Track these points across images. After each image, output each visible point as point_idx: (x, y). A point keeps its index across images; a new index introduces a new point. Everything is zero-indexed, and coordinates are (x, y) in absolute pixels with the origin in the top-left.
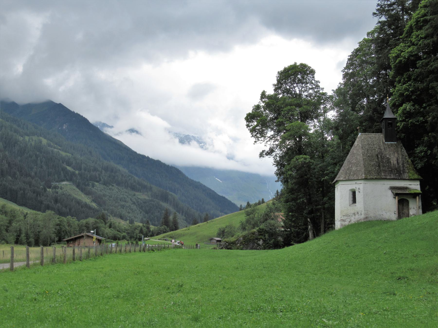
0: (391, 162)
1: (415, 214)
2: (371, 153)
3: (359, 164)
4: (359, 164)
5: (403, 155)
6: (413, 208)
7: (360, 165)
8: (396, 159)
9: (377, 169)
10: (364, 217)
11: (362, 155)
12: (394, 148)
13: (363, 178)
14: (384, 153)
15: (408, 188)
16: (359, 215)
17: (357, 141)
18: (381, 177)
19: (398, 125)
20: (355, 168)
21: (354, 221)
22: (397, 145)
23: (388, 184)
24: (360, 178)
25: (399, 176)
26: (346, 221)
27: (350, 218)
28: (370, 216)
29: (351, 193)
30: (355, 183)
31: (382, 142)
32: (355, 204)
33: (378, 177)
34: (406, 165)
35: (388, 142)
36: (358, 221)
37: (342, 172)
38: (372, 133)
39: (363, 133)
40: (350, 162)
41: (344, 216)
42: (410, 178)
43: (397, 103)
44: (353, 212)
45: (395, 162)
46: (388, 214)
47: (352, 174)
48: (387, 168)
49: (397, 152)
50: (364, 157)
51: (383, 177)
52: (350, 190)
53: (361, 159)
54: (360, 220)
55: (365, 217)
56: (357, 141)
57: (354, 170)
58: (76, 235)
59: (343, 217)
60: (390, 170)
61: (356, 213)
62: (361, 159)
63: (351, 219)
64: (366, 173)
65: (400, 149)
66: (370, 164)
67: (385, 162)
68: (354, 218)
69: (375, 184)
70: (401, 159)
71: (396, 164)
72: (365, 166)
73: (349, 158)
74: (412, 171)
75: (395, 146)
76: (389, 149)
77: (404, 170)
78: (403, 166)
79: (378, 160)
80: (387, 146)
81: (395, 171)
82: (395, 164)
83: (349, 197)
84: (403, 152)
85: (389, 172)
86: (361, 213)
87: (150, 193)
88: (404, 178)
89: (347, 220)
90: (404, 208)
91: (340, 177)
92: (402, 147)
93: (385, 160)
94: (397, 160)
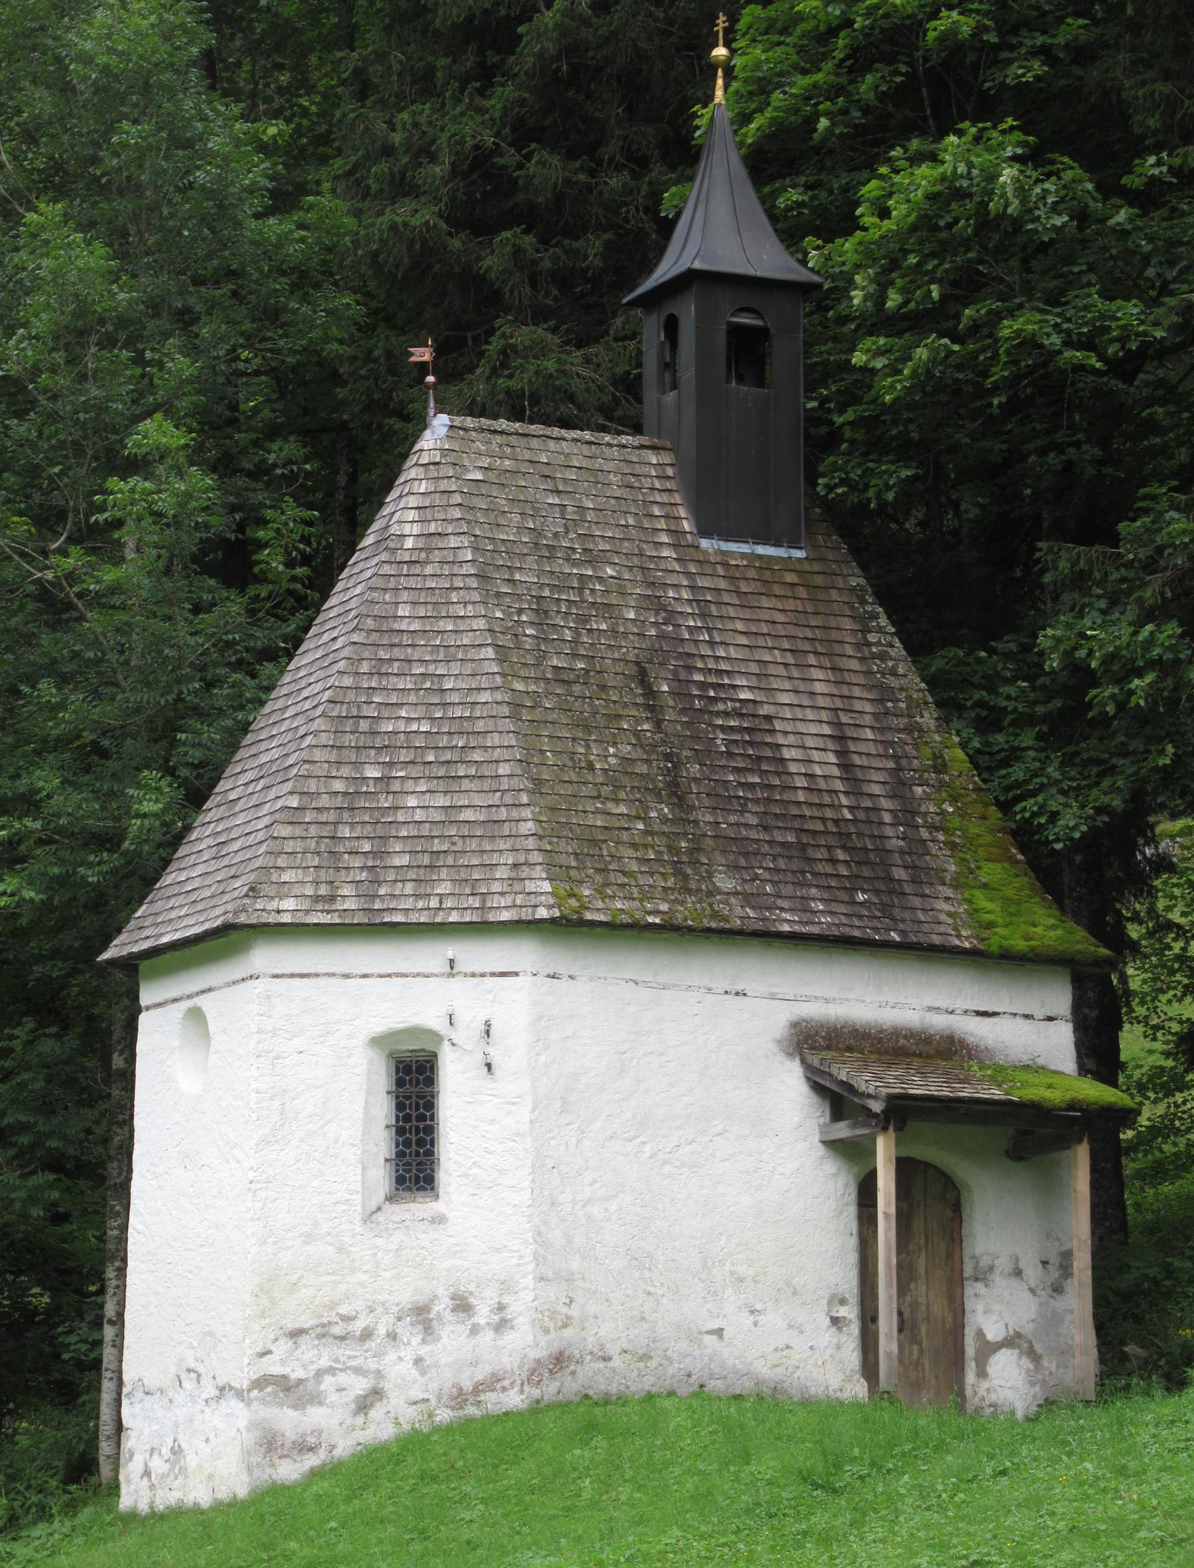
0: (787, 754)
1: (1028, 1329)
2: (575, 642)
3: (477, 756)
4: (477, 756)
5: (884, 694)
6: (1003, 1263)
7: (486, 771)
8: (827, 730)
9: (665, 820)
10: (534, 1354)
11: (490, 652)
12: (790, 604)
13: (542, 913)
14: (705, 650)
15: (962, 1042)
16: (474, 1331)
17: (413, 501)
18: (715, 915)
19: (858, 358)
20: (427, 800)
21: (417, 1393)
22: (819, 580)
23: (773, 997)
24: (505, 916)
25: (885, 908)
26: (316, 1399)
27: (372, 1364)
28: (591, 1343)
29: (382, 1080)
30: (441, 966)
31: (664, 538)
32: (419, 1208)
33: (687, 911)
34: (927, 797)
35: (727, 536)
36: (460, 1398)
37: (285, 831)
38: (556, 431)
39: (469, 422)
40: (364, 725)
41: (296, 1334)
42: (994, 945)
43: (824, 123)
44: (406, 1297)
45: (826, 764)
46: (773, 1320)
47: (405, 860)
48: (753, 820)
49: (830, 654)
50: (519, 686)
51: (740, 914)
52: (377, 1041)
53: (485, 697)
54: (493, 1382)
56: (413, 501)
57: (419, 815)
59: (285, 1345)
60: (791, 838)
61: (437, 1308)
62: (485, 697)
63: (379, 1374)
64: (563, 860)
65: (848, 624)
66: (591, 767)
67: (730, 755)
68: (418, 1361)
69: (648, 985)
70: (869, 734)
71: (839, 786)
72: (538, 782)
73: (347, 681)
74: (991, 872)
75: (802, 592)
76: (748, 614)
77: (917, 847)
78: (907, 814)
79: (658, 724)
80: (722, 584)
81: (833, 861)
82: (822, 784)
83: (367, 1118)
84: (883, 657)
85: (782, 864)
86: (501, 1308)
87: (1060, 626)
88: (936, 940)
89: (328, 1382)
91: (267, 889)
92: (863, 602)
93: (723, 728)
94: (841, 739)
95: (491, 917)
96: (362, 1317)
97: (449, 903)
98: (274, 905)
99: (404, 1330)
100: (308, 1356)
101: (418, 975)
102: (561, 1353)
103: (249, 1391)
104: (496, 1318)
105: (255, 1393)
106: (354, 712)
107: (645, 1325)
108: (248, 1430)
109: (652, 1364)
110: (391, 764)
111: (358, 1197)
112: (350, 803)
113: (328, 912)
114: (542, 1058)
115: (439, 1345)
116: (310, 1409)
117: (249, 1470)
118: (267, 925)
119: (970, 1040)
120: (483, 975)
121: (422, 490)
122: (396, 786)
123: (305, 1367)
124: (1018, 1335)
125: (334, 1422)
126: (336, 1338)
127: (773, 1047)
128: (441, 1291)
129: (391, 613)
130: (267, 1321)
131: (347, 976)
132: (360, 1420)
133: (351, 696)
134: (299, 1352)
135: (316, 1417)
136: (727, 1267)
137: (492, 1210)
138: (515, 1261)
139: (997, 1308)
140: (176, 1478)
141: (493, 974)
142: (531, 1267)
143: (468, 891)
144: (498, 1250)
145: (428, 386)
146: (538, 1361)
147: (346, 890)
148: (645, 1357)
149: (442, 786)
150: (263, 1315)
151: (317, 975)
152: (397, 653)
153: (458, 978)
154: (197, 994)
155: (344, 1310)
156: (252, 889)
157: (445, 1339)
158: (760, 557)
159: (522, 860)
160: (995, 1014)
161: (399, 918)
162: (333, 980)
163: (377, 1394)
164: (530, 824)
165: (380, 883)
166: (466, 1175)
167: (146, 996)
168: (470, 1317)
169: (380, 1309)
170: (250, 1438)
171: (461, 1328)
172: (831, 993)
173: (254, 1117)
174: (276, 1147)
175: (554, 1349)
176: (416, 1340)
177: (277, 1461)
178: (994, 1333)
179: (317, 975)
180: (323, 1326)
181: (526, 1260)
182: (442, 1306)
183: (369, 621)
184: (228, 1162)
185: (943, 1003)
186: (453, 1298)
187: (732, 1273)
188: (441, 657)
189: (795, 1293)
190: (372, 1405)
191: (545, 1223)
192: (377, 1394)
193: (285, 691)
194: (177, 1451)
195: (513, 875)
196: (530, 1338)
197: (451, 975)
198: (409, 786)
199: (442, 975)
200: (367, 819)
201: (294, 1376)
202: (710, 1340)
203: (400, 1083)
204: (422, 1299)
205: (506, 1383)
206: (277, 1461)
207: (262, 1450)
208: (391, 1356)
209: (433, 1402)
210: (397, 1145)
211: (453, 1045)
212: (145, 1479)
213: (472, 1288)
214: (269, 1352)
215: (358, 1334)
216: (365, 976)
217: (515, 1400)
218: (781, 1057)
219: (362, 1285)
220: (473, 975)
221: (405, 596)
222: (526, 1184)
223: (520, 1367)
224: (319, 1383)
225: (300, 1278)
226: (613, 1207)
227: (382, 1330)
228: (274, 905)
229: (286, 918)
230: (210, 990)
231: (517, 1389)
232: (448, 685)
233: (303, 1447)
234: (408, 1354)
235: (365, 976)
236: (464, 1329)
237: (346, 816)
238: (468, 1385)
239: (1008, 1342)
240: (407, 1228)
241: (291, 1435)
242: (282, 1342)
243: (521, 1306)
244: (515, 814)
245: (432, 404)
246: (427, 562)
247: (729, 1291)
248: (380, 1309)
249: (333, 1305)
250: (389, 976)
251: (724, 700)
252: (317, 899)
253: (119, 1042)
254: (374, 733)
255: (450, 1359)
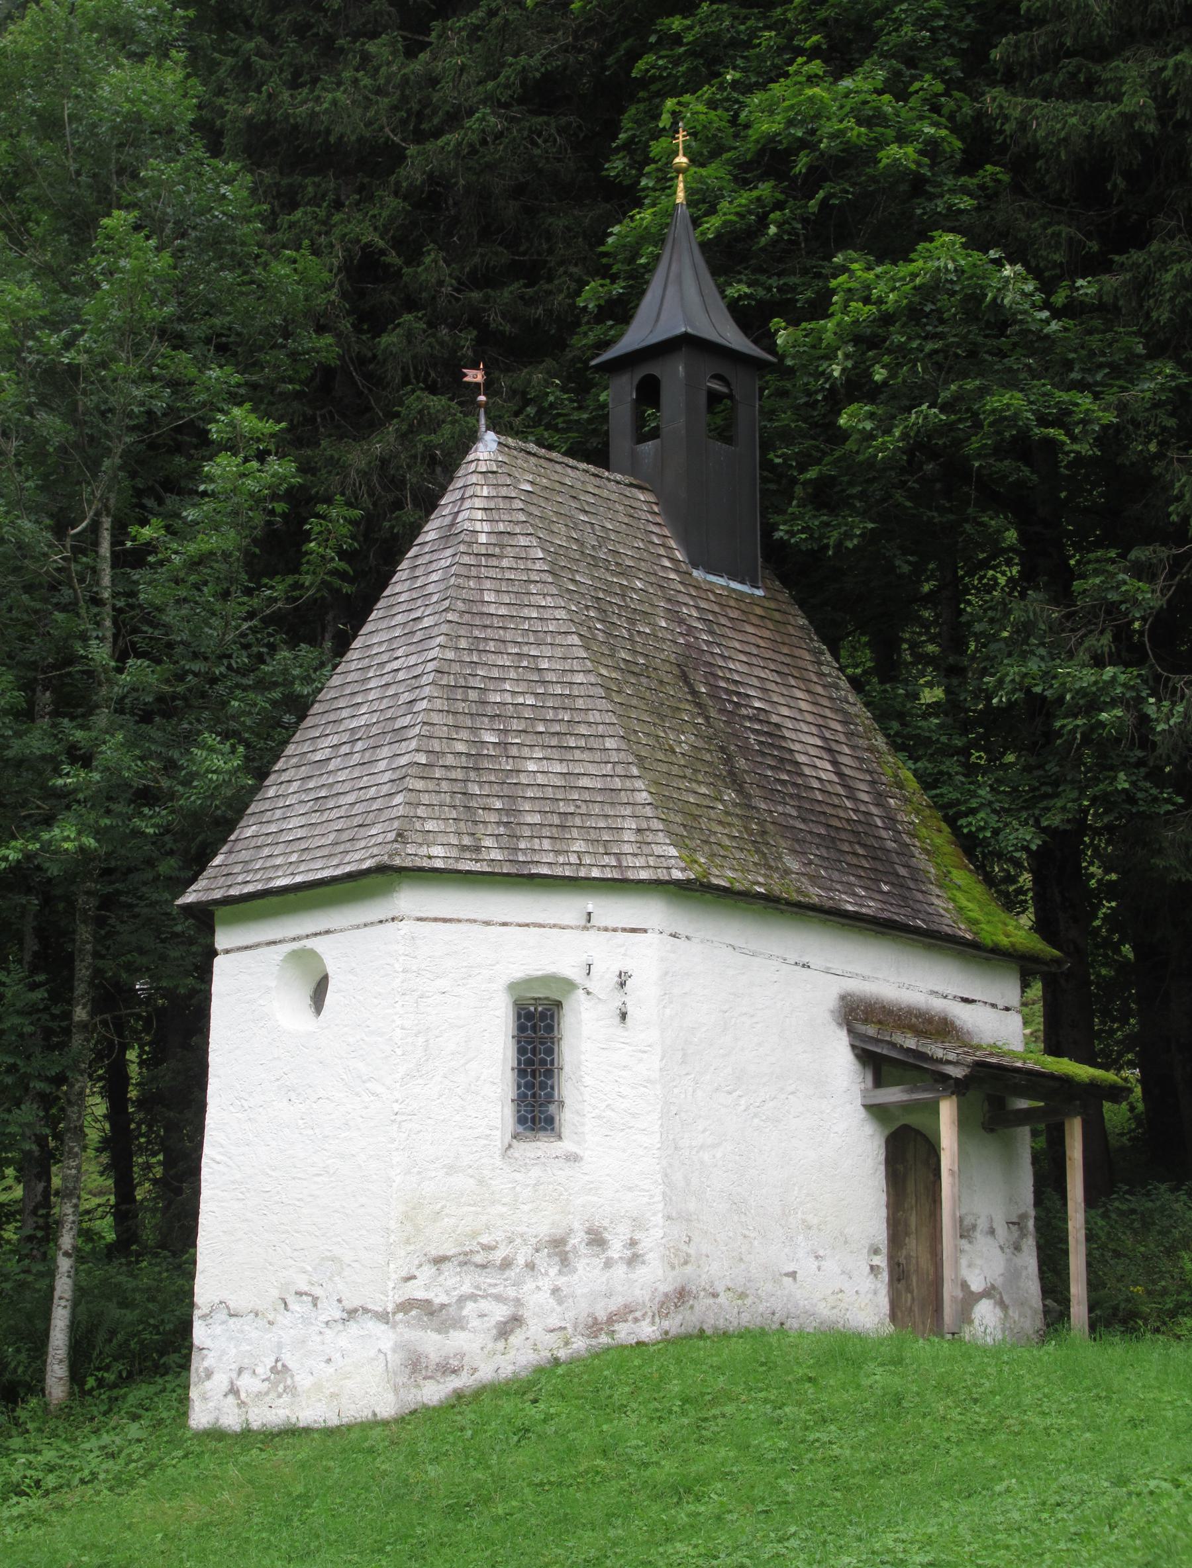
1: (999, 1282)
4: (583, 730)
6: (982, 1224)
13: (677, 875)
15: (952, 1023)
16: (608, 1264)
20: (545, 766)
21: (554, 1322)
24: (644, 875)
26: (458, 1323)
27: (511, 1292)
28: (704, 1280)
32: (542, 1147)
35: (710, 570)
36: (594, 1327)
39: (510, 441)
40: (473, 695)
41: (439, 1261)
44: (544, 1229)
46: (830, 1265)
52: (512, 987)
54: (625, 1313)
55: (664, 1288)
56: (478, 503)
57: (541, 779)
58: (1091, 1200)
59: (428, 1271)
61: (573, 1241)
62: (579, 678)
63: (518, 1302)
68: (555, 1291)
83: (505, 1060)
86: (633, 1243)
89: (470, 1308)
90: (907, 1225)
92: (812, 640)
93: (754, 731)
95: (631, 875)
96: (502, 1247)
97: (587, 860)
98: (424, 851)
99: (541, 1260)
100: (451, 1282)
101: (555, 926)
102: (683, 1289)
103: (394, 1313)
104: (629, 1253)
105: (400, 1316)
106: (462, 682)
107: (743, 1266)
108: (394, 1351)
109: (748, 1301)
110: (505, 731)
111: (498, 1133)
112: (476, 761)
113: (477, 861)
114: (668, 1011)
115: (576, 1277)
116: (453, 1334)
117: (396, 1390)
118: (421, 869)
119: (958, 1023)
120: (615, 930)
121: (485, 493)
122: (514, 751)
123: (447, 1293)
124: (993, 1287)
125: (476, 1346)
126: (477, 1266)
127: (828, 1017)
128: (576, 1226)
129: (478, 598)
130: (412, 1248)
131: (487, 923)
132: (501, 1345)
133: (456, 668)
134: (442, 1278)
135: (458, 1340)
136: (800, 1215)
137: (624, 1151)
138: (646, 1200)
139: (979, 1262)
140: (280, 1396)
141: (624, 930)
142: (660, 1206)
143: (601, 850)
144: (630, 1189)
145: (479, 405)
146: (666, 1295)
147: (488, 842)
148: (742, 1296)
149: (555, 754)
150: (408, 1242)
151: (459, 921)
152: (490, 633)
153: (592, 932)
154: (307, 936)
155: (485, 1239)
156: (399, 835)
157: (580, 1271)
158: (734, 590)
159: (644, 826)
160: (973, 1001)
161: (545, 870)
162: (475, 927)
163: (516, 1321)
164: (645, 794)
165: (518, 838)
166: (599, 1117)
167: (222, 940)
168: (604, 1251)
169: (519, 1241)
170: (395, 1359)
171: (596, 1261)
172: (867, 972)
173: (399, 1052)
174: (420, 1081)
175: (678, 1285)
176: (553, 1271)
177: (421, 1382)
178: (976, 1286)
179: (459, 921)
180: (466, 1254)
181: (656, 1199)
182: (577, 1240)
183: (459, 603)
184: (357, 1094)
185: (938, 988)
186: (588, 1233)
187: (804, 1221)
188: (532, 640)
189: (846, 1242)
190: (512, 1331)
191: (670, 1165)
192: (516, 1321)
193: (353, 666)
194: (280, 1371)
195: (639, 839)
196: (660, 1272)
197: (585, 928)
198: (526, 752)
199: (577, 927)
200: (493, 779)
201: (437, 1301)
202: (787, 1281)
203: (521, 1028)
204: (559, 1232)
205: (638, 1314)
206: (421, 1382)
207: (408, 1371)
208: (530, 1285)
209: (570, 1330)
210: (519, 1087)
211: (588, 993)
212: (231, 1398)
213: (606, 1223)
214: (414, 1277)
215: (498, 1263)
216: (504, 924)
217: (647, 1331)
218: (833, 1026)
219: (502, 1216)
220: (606, 929)
221: (488, 584)
222: (656, 1128)
223: (651, 1300)
224: (462, 1308)
225: (444, 1207)
226: (719, 1155)
227: (521, 1261)
228: (424, 851)
229: (439, 864)
230: (327, 932)
231: (648, 1320)
232: (545, 665)
233: (447, 1369)
234: (546, 1284)
235: (504, 924)
236: (599, 1262)
237: (472, 775)
238: (602, 1316)
239: (987, 1293)
240: (544, 1164)
241: (434, 1358)
242: (425, 1268)
243: (650, 1242)
244: (628, 784)
245: (483, 421)
246: (500, 557)
247: (801, 1238)
248: (519, 1241)
249: (475, 1235)
250: (527, 925)
251: (746, 706)
252: (464, 848)
253: (83, 996)
254: (484, 703)
255: (586, 1290)
